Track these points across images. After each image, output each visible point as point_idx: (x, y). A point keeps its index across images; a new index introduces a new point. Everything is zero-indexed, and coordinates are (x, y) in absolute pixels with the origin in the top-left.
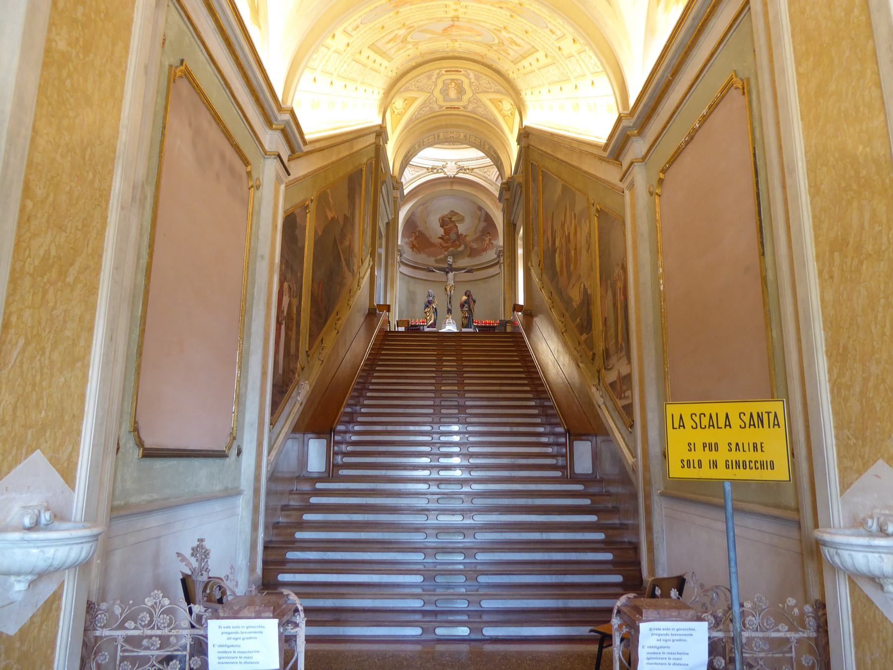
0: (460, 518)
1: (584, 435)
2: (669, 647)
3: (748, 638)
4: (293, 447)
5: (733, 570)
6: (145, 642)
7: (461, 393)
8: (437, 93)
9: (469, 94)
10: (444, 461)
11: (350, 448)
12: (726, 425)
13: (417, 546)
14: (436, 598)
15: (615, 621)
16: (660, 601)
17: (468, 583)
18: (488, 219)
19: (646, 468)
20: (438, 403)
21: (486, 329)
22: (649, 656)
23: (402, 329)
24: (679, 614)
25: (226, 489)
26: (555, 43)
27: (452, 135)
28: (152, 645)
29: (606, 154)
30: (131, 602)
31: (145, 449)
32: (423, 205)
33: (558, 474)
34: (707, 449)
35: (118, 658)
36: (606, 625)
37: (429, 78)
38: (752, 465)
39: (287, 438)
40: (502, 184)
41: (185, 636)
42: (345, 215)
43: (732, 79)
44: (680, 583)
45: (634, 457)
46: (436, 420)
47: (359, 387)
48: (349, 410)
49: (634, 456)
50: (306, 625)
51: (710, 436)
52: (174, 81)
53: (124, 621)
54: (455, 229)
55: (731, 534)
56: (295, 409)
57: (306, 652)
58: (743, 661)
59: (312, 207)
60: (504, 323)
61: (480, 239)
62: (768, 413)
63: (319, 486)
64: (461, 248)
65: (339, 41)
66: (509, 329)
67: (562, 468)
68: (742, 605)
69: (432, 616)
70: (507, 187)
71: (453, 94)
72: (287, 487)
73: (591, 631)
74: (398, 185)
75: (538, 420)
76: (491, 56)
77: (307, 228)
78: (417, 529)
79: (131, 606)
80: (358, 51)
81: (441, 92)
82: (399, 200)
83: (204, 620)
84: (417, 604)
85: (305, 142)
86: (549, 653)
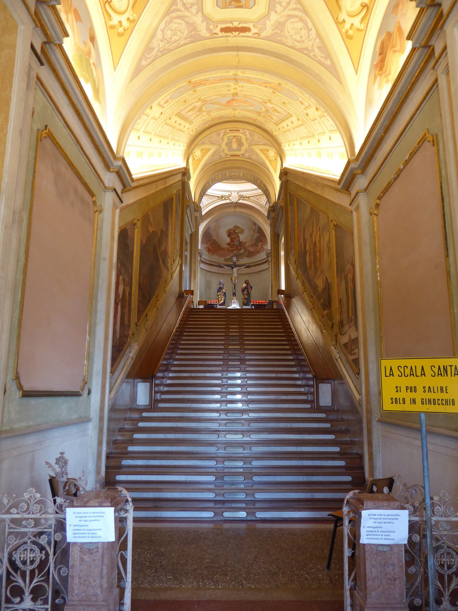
0: (241, 436)
1: (326, 379)
2: (381, 528)
3: (435, 521)
4: (126, 388)
5: (426, 474)
6: (24, 523)
7: (242, 351)
8: (224, 146)
9: (246, 146)
10: (230, 397)
11: (166, 389)
12: (422, 375)
13: (212, 456)
14: (224, 491)
15: (345, 509)
16: (376, 495)
17: (246, 481)
18: (260, 231)
19: (368, 402)
20: (226, 357)
21: (259, 307)
22: (368, 533)
23: (201, 307)
24: (389, 504)
25: (80, 417)
26: (304, 111)
27: (234, 174)
28: (29, 524)
29: (340, 187)
30: (14, 496)
31: (24, 391)
32: (216, 221)
33: (308, 406)
34: (409, 390)
35: (7, 533)
36: (339, 511)
37: (218, 135)
38: (440, 402)
39: (122, 382)
40: (269, 207)
41: (52, 518)
42: (161, 229)
43: (425, 135)
44: (390, 482)
45: (360, 395)
46: (225, 369)
47: (172, 347)
48: (165, 362)
49: (360, 394)
50: (134, 511)
51: (411, 381)
52: (41, 140)
53: (10, 508)
54: (237, 239)
55: (425, 449)
56: (128, 363)
57: (134, 529)
58: (432, 536)
59: (139, 224)
60: (271, 303)
61: (255, 245)
62: (451, 366)
63: (145, 414)
64: (242, 251)
65: (156, 111)
66: (275, 306)
67: (311, 402)
68: (432, 499)
69: (220, 504)
70: (273, 209)
71: (235, 146)
72: (122, 415)
73: (329, 515)
74: (198, 209)
75: (295, 369)
76: (261, 120)
77: (135, 238)
78: (212, 444)
79: (14, 498)
80: (168, 117)
81: (227, 144)
82: (199, 218)
83: (63, 508)
84: (211, 496)
85: (132, 180)
86: (301, 529)
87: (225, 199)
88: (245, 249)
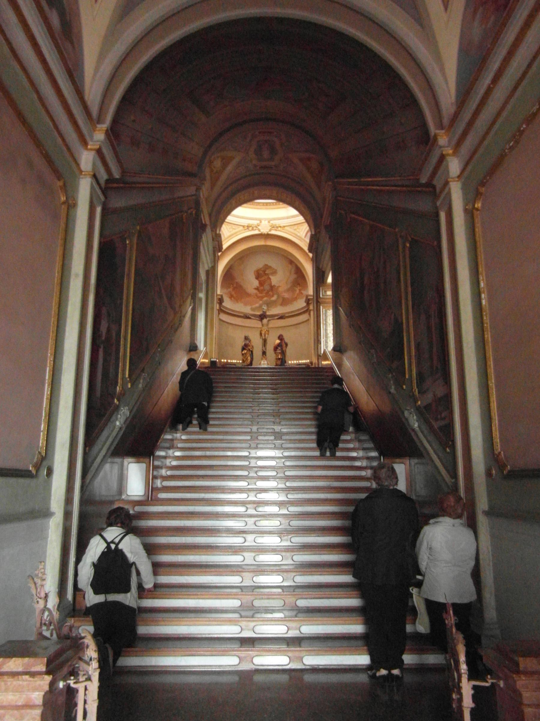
10: (261, 484)
45: (452, 477)
64: (274, 298)
87: (253, 229)
88: (279, 297)
